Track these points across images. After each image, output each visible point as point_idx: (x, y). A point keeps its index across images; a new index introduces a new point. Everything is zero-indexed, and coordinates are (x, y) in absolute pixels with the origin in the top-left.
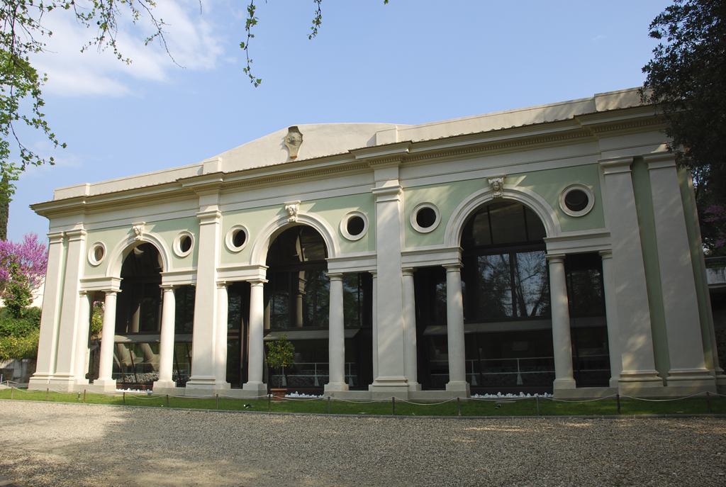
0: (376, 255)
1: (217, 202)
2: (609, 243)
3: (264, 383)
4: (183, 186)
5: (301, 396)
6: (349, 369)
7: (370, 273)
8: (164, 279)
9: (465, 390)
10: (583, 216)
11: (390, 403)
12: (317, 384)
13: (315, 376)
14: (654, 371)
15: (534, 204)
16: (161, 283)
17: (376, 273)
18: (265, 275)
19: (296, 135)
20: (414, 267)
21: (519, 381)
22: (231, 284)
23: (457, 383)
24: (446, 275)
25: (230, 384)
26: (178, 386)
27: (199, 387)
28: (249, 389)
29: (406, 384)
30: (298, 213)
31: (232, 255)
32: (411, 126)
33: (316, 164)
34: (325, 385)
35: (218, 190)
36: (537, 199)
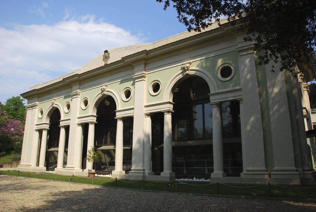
0: (134, 108)
1: (78, 88)
2: (242, 94)
3: (93, 169)
4: (66, 82)
5: (201, 180)
6: (225, 163)
7: (237, 101)
8: (117, 114)
9: (169, 176)
10: (229, 80)
11: (72, 176)
12: (206, 172)
13: (206, 168)
14: (295, 168)
15: (204, 76)
16: (60, 125)
17: (242, 100)
18: (96, 119)
19: (107, 54)
20: (150, 113)
21: (185, 172)
22: (84, 124)
23: (167, 172)
24: (239, 105)
25: (174, 173)
26: (126, 173)
27: (68, 170)
28: (57, 170)
29: (142, 172)
30: (190, 69)
31: (86, 110)
32: (151, 43)
33: (112, 66)
34: (211, 173)
35: (78, 82)
36: (207, 74)
